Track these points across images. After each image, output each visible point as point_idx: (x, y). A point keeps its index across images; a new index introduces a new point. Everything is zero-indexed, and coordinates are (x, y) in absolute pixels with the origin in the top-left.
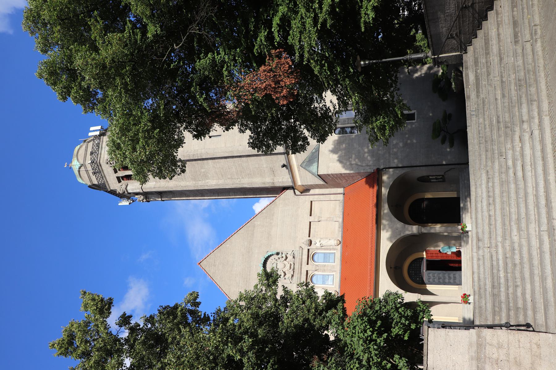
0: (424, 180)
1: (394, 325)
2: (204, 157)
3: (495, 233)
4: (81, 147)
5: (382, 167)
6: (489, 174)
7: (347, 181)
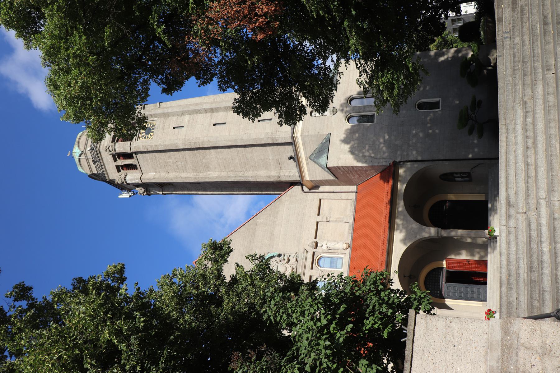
0: (448, 177)
1: (369, 314)
2: (206, 146)
3: (535, 189)
4: (82, 134)
5: (398, 160)
6: (527, 105)
7: (360, 176)
